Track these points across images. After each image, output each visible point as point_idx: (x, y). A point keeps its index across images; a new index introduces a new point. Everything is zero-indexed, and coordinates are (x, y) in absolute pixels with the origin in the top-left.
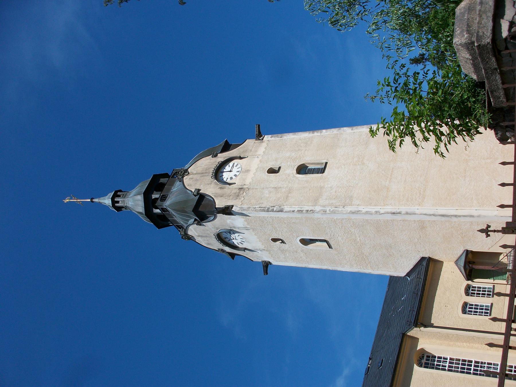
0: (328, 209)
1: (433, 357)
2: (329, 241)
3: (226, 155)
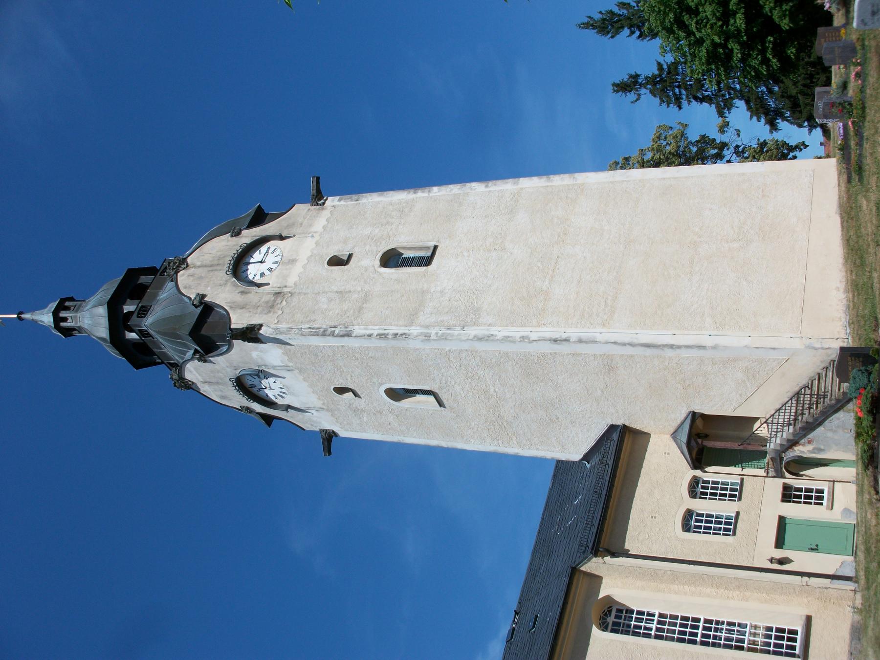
0: (433, 332)
1: (628, 612)
2: (438, 392)
3: (255, 232)
